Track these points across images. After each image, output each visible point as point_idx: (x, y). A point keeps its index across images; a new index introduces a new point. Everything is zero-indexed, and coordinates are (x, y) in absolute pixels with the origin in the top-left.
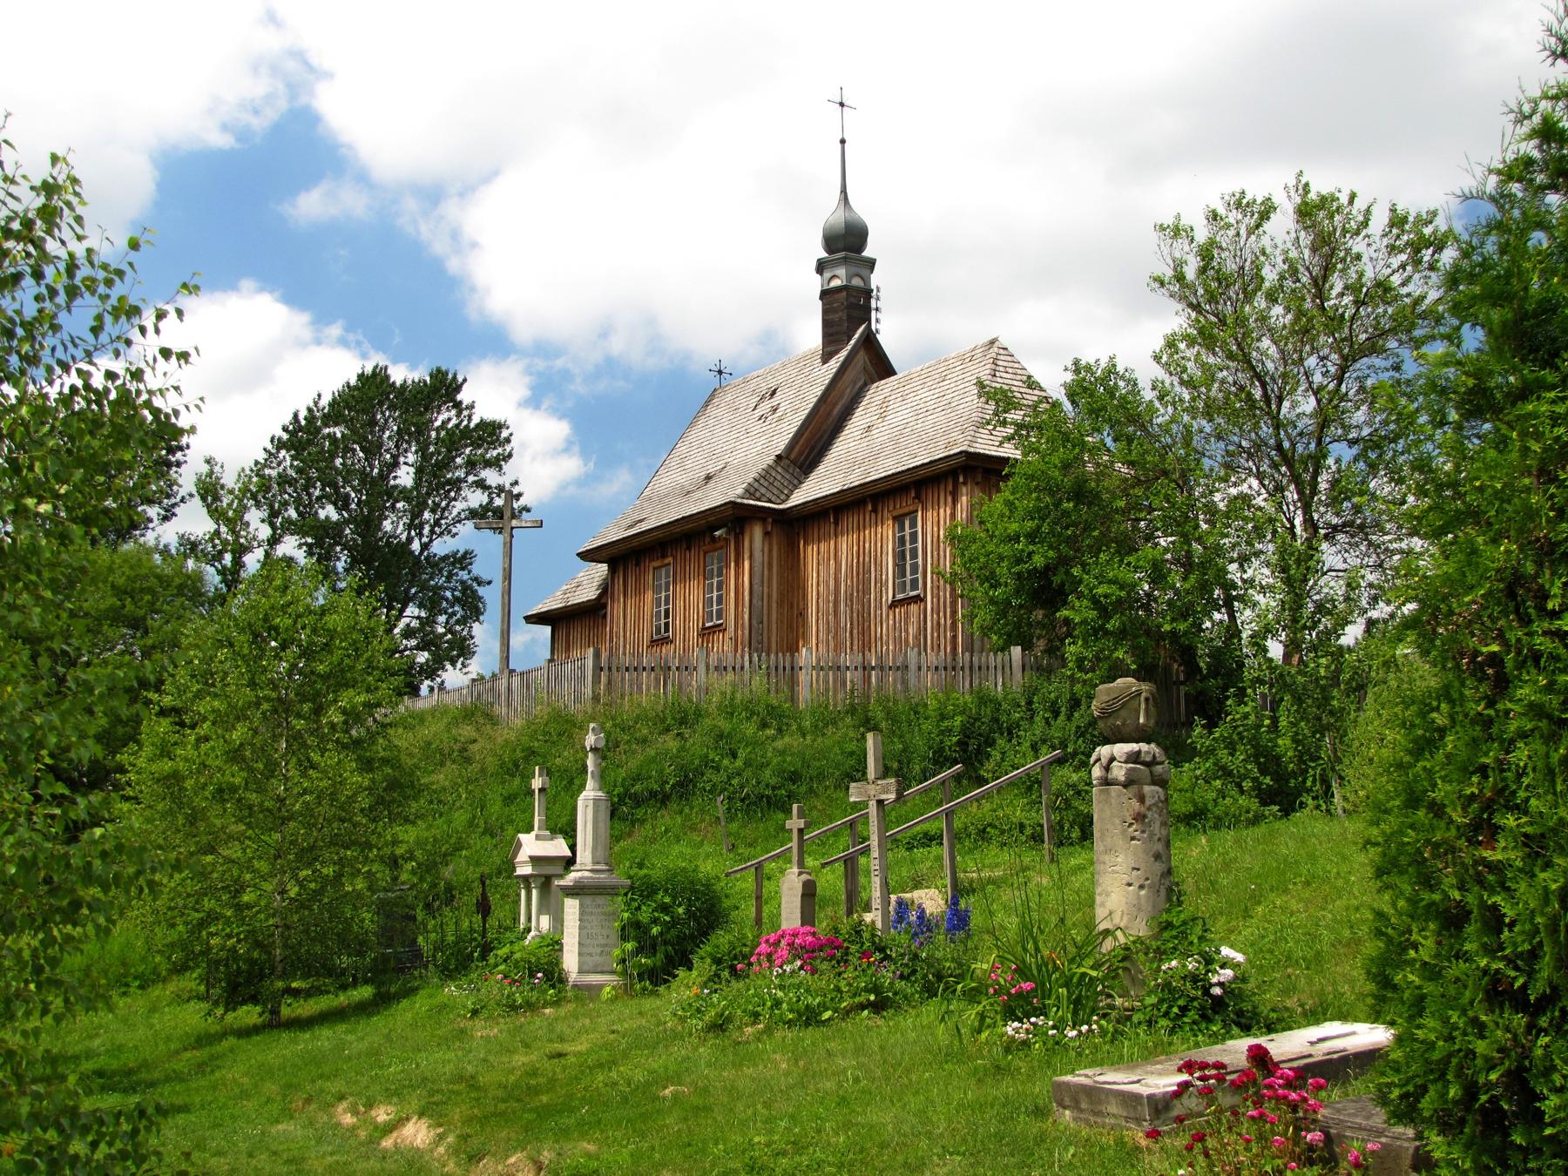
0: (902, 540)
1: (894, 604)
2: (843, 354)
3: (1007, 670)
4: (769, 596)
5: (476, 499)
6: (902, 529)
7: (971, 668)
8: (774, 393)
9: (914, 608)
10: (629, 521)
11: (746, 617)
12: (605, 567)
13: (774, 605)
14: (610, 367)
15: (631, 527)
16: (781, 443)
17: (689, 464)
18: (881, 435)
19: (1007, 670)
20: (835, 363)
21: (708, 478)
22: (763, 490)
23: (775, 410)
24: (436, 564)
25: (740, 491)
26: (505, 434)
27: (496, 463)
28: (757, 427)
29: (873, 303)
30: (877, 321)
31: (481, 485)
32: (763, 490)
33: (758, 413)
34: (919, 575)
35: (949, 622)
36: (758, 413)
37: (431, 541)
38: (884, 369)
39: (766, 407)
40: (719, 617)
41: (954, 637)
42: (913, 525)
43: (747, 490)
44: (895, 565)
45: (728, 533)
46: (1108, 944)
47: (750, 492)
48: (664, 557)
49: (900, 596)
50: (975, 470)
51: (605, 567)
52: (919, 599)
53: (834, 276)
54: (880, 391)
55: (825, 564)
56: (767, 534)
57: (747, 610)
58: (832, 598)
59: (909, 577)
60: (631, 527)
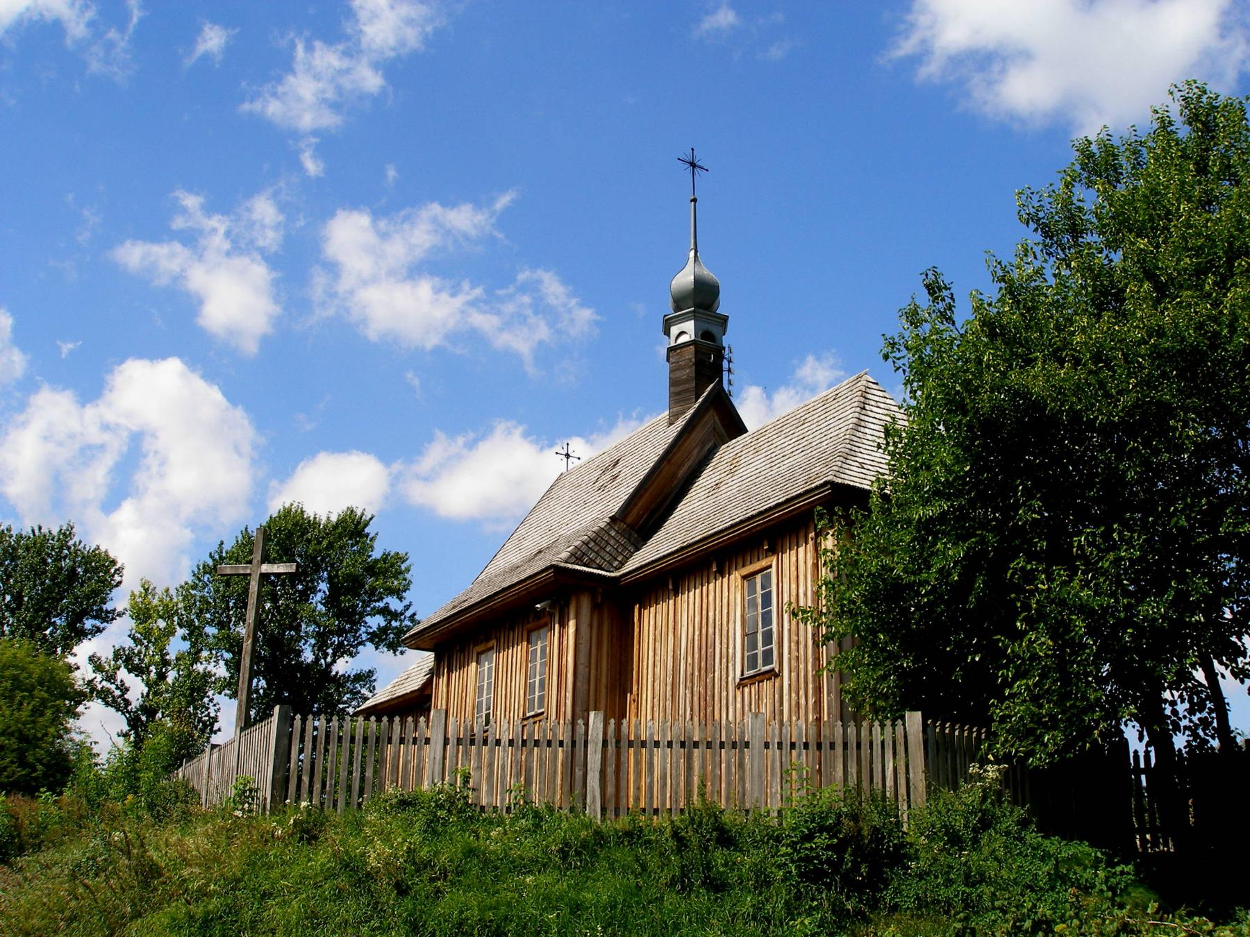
0: (753, 603)
1: (741, 685)
2: (692, 411)
3: (901, 749)
4: (598, 680)
5: (376, 622)
6: (753, 590)
7: (845, 745)
8: (617, 463)
9: (766, 686)
11: (569, 702)
12: (430, 656)
13: (604, 690)
14: (30, 20)
16: (615, 506)
17: (525, 543)
18: (725, 493)
19: (901, 749)
20: (680, 423)
21: (540, 552)
23: (615, 477)
24: (339, 681)
25: (564, 555)
26: (403, 567)
27: (398, 593)
29: (725, 364)
30: (730, 383)
31: (385, 611)
34: (774, 646)
35: (811, 701)
37: (334, 661)
38: (736, 427)
39: (608, 476)
40: (541, 705)
41: (818, 703)
43: (573, 554)
44: (744, 635)
45: (552, 606)
46: (300, 48)
47: (576, 556)
48: (488, 640)
49: (747, 673)
50: (839, 502)
51: (430, 656)
52: (773, 675)
53: (682, 333)
54: (726, 452)
55: (663, 631)
56: (595, 607)
57: (569, 695)
58: (669, 681)
59: (760, 648)
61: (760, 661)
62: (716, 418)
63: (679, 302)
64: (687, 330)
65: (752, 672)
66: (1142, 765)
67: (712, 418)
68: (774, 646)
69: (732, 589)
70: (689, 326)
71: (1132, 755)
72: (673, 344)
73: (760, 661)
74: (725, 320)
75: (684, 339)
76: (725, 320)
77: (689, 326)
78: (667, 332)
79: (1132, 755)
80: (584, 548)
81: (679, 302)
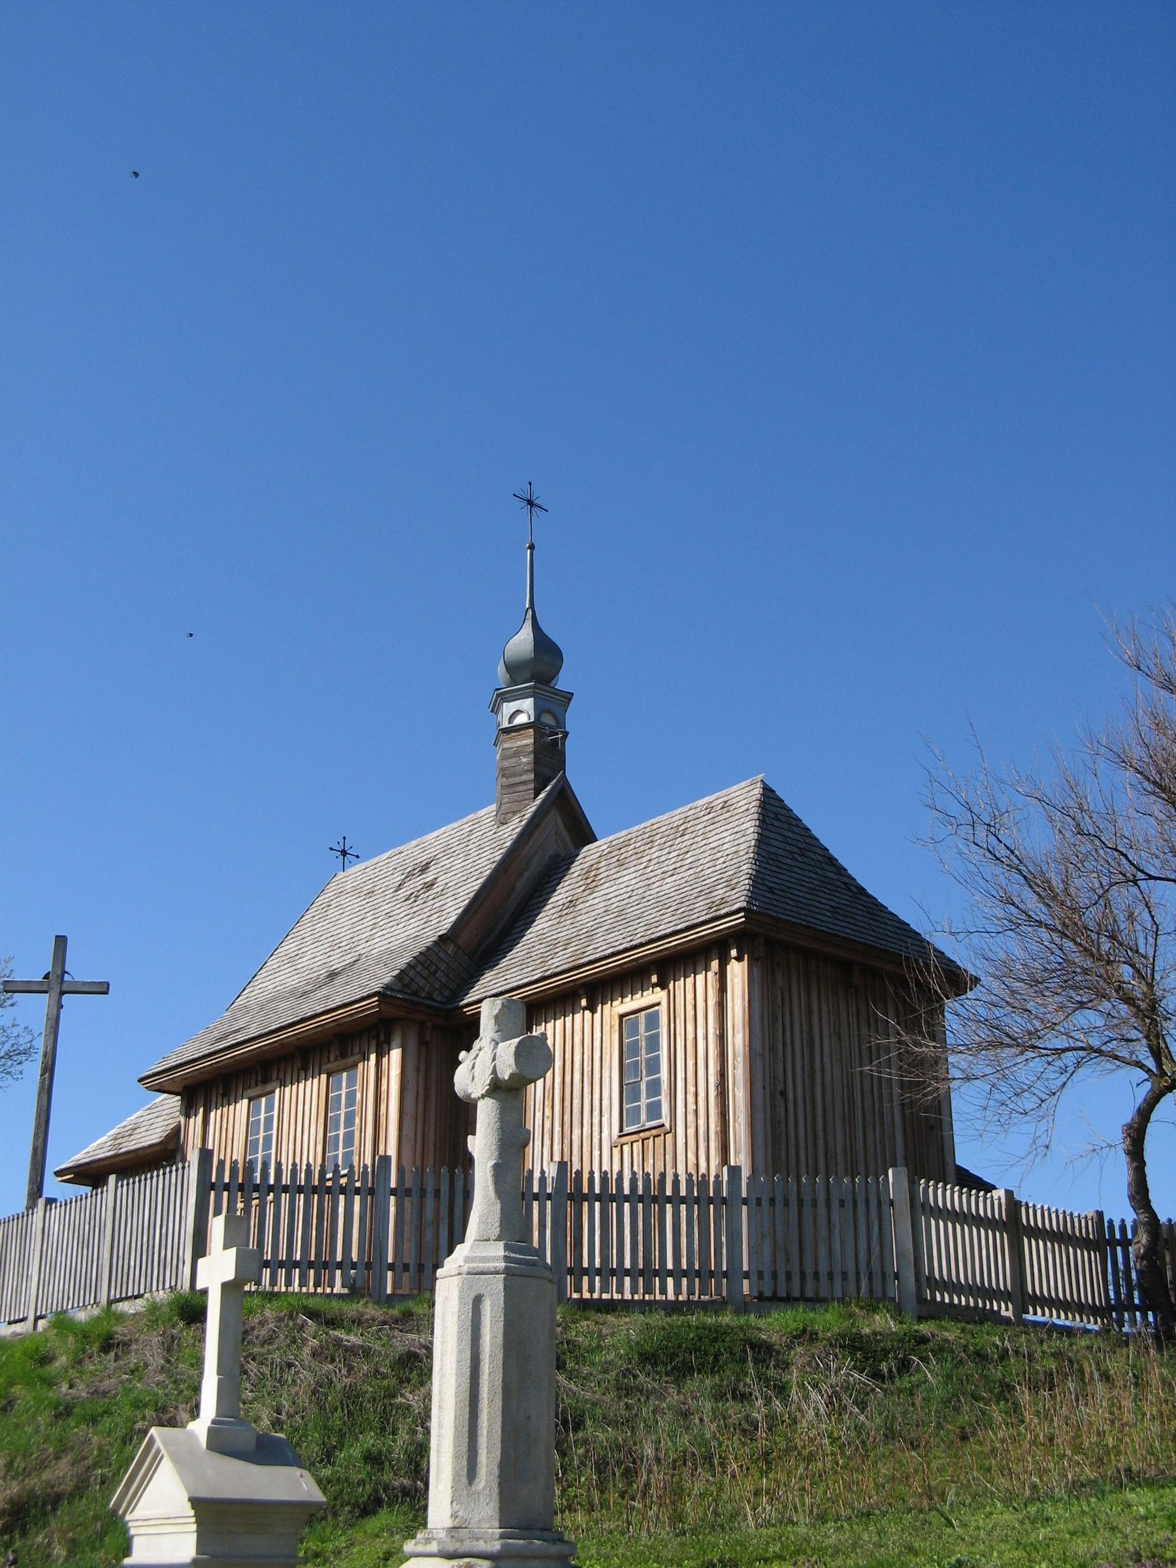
10: (216, 1034)
13: (432, 1147)
15: (221, 1039)
16: (429, 937)
17: (304, 962)
20: (515, 826)
21: (333, 975)
22: (422, 982)
23: (430, 886)
28: (403, 910)
32: (422, 982)
33: (403, 893)
36: (403, 893)
39: (418, 882)
42: (269, 1108)
48: (266, 1081)
53: (518, 712)
54: (590, 854)
60: (221, 1039)
61: (643, 1117)
62: (559, 819)
63: (515, 669)
64: (523, 710)
65: (633, 1129)
66: (1118, 1236)
67: (555, 819)
68: (356, 1128)
69: (606, 1028)
70: (528, 704)
71: (1106, 1224)
72: (505, 724)
73: (643, 1117)
74: (569, 696)
75: (521, 719)
76: (569, 696)
77: (528, 704)
78: (495, 709)
79: (1106, 1224)
80: (412, 973)
81: (515, 669)
